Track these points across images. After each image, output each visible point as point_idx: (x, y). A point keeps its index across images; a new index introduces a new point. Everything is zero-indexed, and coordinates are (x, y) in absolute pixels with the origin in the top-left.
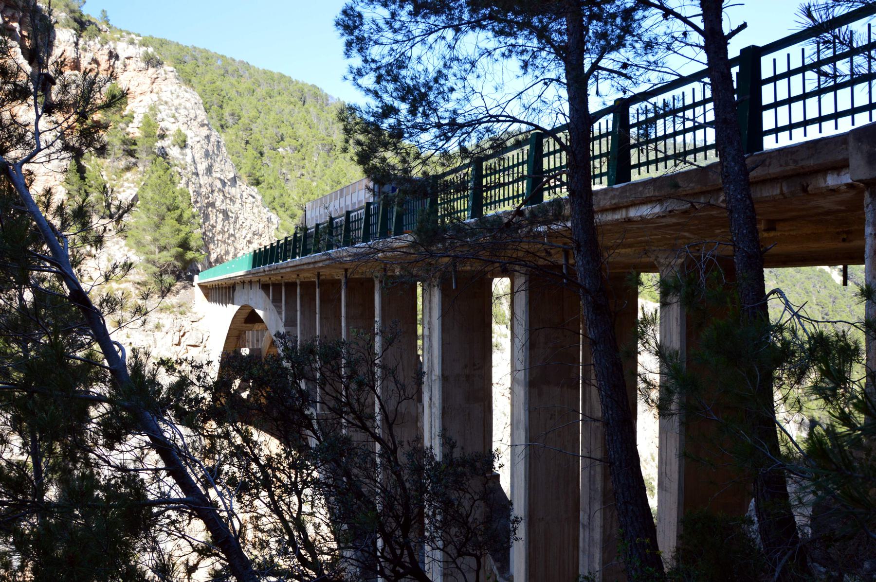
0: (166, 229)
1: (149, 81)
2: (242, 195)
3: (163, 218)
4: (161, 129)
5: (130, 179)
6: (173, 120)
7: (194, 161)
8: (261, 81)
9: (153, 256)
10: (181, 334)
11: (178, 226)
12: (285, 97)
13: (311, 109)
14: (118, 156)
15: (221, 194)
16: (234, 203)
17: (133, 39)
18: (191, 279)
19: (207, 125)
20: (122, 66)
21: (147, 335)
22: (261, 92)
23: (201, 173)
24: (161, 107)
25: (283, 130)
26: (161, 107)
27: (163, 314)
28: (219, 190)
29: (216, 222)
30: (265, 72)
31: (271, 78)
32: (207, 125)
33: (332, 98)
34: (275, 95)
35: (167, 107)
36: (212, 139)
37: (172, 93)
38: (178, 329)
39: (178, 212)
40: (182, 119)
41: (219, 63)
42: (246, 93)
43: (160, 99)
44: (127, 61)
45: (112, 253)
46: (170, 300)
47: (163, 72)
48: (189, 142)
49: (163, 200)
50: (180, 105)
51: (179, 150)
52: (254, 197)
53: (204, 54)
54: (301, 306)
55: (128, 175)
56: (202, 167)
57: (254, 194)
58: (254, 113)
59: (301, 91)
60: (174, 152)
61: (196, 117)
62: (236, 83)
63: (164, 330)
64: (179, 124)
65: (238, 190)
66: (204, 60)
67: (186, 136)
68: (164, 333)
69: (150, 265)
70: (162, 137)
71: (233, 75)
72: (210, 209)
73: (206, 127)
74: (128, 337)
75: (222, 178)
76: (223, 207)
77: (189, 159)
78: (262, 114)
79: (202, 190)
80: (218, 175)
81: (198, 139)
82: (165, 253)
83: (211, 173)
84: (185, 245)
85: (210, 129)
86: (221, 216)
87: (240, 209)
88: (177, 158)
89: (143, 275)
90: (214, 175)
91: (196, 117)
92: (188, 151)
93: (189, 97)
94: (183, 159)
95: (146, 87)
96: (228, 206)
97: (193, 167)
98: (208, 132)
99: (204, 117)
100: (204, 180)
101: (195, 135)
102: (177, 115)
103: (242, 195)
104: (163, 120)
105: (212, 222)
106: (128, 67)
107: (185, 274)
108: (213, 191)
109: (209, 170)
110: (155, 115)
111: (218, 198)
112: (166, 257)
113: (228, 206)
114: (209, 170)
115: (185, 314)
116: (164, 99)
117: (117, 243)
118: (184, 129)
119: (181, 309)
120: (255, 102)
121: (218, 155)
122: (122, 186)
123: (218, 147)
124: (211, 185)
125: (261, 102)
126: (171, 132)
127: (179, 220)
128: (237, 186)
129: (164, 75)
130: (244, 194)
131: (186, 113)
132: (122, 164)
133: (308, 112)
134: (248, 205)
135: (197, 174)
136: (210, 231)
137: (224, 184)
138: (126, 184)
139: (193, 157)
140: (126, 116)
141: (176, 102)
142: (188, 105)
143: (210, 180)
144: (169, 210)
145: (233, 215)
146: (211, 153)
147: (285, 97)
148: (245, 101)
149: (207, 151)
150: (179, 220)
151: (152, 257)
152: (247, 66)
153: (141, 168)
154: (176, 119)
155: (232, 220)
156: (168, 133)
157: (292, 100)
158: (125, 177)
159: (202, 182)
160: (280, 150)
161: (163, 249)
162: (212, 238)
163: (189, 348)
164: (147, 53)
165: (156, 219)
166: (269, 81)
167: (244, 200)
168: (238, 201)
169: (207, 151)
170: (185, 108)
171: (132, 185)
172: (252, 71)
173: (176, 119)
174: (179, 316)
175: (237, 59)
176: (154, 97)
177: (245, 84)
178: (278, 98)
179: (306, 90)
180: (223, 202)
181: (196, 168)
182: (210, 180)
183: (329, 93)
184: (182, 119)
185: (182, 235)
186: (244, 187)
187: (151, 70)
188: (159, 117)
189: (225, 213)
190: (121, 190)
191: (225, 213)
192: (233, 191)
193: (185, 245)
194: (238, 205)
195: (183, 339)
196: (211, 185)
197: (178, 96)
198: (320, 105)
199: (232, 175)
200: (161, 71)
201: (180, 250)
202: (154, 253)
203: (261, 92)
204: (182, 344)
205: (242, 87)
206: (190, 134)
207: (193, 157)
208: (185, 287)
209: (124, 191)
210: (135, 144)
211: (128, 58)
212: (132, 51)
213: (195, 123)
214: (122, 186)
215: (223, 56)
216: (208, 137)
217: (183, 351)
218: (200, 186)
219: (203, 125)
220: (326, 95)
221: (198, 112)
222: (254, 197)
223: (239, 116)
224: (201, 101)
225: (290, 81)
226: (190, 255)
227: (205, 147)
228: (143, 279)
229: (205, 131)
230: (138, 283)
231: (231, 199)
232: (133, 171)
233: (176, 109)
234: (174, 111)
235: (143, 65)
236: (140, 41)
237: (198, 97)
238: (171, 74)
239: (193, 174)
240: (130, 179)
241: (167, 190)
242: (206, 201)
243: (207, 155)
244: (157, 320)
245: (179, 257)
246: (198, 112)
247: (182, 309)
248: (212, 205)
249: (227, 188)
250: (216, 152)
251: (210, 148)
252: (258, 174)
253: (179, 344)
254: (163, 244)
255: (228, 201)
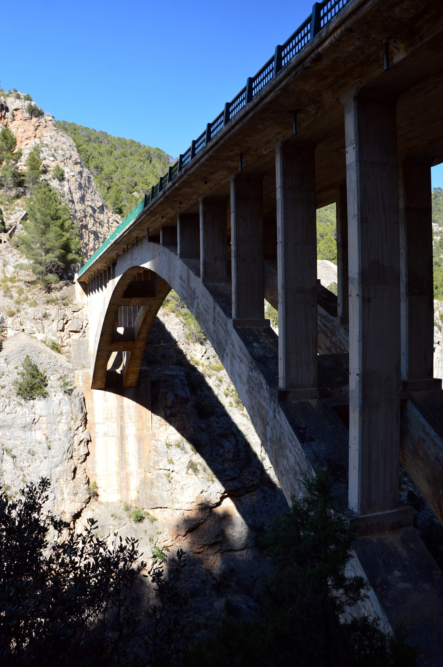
0: (51, 235)
1: (32, 128)
2: (108, 221)
3: (47, 226)
4: (44, 166)
5: (20, 204)
6: (52, 159)
7: (70, 191)
8: (117, 146)
9: (40, 258)
10: (65, 322)
11: (60, 232)
12: (136, 157)
13: (157, 165)
14: (10, 186)
15: (92, 219)
16: (103, 226)
17: (19, 94)
18: (72, 278)
19: (80, 163)
20: (11, 116)
21: (37, 323)
22: (117, 153)
23: (76, 201)
24: (43, 149)
25: (136, 179)
26: (43, 149)
27: (50, 306)
28: (91, 215)
29: (89, 241)
30: (119, 139)
31: (123, 142)
32: (80, 163)
33: (172, 158)
34: (128, 155)
35: (47, 149)
36: (84, 175)
37: (51, 138)
38: (62, 317)
39: (60, 221)
40: (60, 158)
41: (84, 133)
42: (106, 154)
43: (42, 142)
44: (15, 113)
45: (7, 260)
46: (55, 295)
47: (44, 121)
48: (66, 176)
49: (48, 211)
50: (58, 147)
51: (58, 182)
52: (118, 223)
53: (72, 126)
54: (204, 223)
55: (18, 201)
56: (77, 196)
57: (118, 220)
58: (113, 168)
59: (148, 152)
60: (55, 184)
61: (71, 156)
62: (98, 147)
63: (51, 318)
64: (58, 162)
65: (105, 216)
66: (72, 131)
67: (63, 172)
68: (50, 321)
69: (38, 265)
70: (45, 172)
71: (95, 142)
72: (84, 230)
73: (79, 165)
74: (21, 325)
75: (93, 205)
76: (94, 229)
77: (66, 189)
78: (119, 169)
79: (77, 214)
80: (90, 203)
81: (72, 174)
82: (50, 255)
83: (84, 201)
84: (66, 248)
85: (82, 167)
86: (92, 236)
87: (107, 232)
88: (57, 189)
89: (32, 276)
90: (87, 203)
91: (71, 156)
92: (65, 183)
93: (65, 141)
94: (62, 189)
95: (30, 133)
96: (98, 229)
97: (69, 196)
98: (81, 169)
99: (77, 157)
100: (78, 206)
101: (70, 171)
102: (56, 154)
103: (108, 221)
104: (45, 159)
105: (86, 241)
106: (16, 117)
107: (67, 275)
108: (85, 216)
109: (82, 199)
110: (38, 155)
111: (90, 222)
112: (51, 257)
113: (98, 229)
114: (82, 199)
115: (67, 305)
116: (45, 142)
117: (11, 252)
118: (61, 166)
119: (64, 302)
120: (113, 160)
121: (89, 188)
122: (14, 209)
123: (89, 181)
124: (84, 211)
125: (117, 160)
126: (52, 169)
127: (62, 226)
128: (105, 213)
129: (44, 124)
130: (110, 219)
131: (63, 153)
132: (14, 193)
133: (154, 167)
134: (113, 229)
135: (73, 202)
136: (84, 248)
137: (94, 211)
138: (17, 208)
139: (70, 188)
140: (15, 154)
141: (55, 145)
142: (65, 147)
143: (83, 207)
144: (53, 219)
145: (102, 236)
146: (83, 185)
147: (136, 157)
148: (105, 160)
149: (80, 184)
150: (62, 226)
151: (40, 258)
152: (105, 135)
153: (28, 196)
154: (55, 158)
155: (101, 240)
156: (49, 169)
157: (142, 159)
158: (16, 203)
159: (77, 208)
160: (135, 194)
161: (47, 251)
162: (86, 254)
163: (71, 333)
164: (30, 105)
165: (42, 227)
166: (123, 146)
167: (110, 224)
168: (106, 225)
169: (80, 184)
170: (62, 149)
171: (22, 209)
172: (109, 138)
173: (55, 158)
174: (63, 307)
175: (98, 130)
176: (37, 141)
177: (104, 148)
178: (131, 157)
179: (152, 152)
180: (94, 225)
181: (72, 197)
182: (83, 207)
183: (170, 154)
184: (60, 158)
185: (64, 239)
186: (110, 214)
187: (34, 120)
188: (41, 155)
189: (95, 234)
190: (13, 212)
191: (95, 234)
192: (101, 217)
193: (66, 248)
194: (105, 228)
195: (66, 326)
196: (84, 211)
197: (56, 140)
198: (163, 163)
199: (100, 204)
200: (42, 120)
201: (63, 251)
202: (42, 256)
203: (117, 153)
204: (65, 331)
205: (103, 150)
206: (66, 170)
207: (70, 188)
208: (67, 285)
209: (15, 213)
210: (24, 176)
211: (16, 110)
212: (18, 104)
213: (70, 162)
214: (14, 209)
215: (86, 128)
216: (81, 173)
217: (67, 336)
218: (76, 211)
219: (76, 163)
220: (168, 155)
221: (73, 153)
222: (118, 223)
223: (101, 168)
224: (75, 145)
225: (139, 146)
226: (71, 256)
227: (79, 180)
228: (33, 279)
229: (78, 168)
230: (29, 282)
231: (100, 224)
232: (23, 198)
233: (55, 150)
234: (53, 152)
235: (28, 115)
236: (25, 97)
237: (72, 141)
238: (50, 122)
239: (70, 201)
240: (20, 204)
241: (51, 203)
242: (81, 223)
243: (80, 187)
244: (45, 310)
245: (62, 258)
246: (73, 153)
247: (65, 302)
248: (86, 227)
249: (97, 214)
250: (87, 185)
251: (83, 182)
252: (120, 204)
253: (63, 330)
254: (48, 247)
255: (98, 225)
